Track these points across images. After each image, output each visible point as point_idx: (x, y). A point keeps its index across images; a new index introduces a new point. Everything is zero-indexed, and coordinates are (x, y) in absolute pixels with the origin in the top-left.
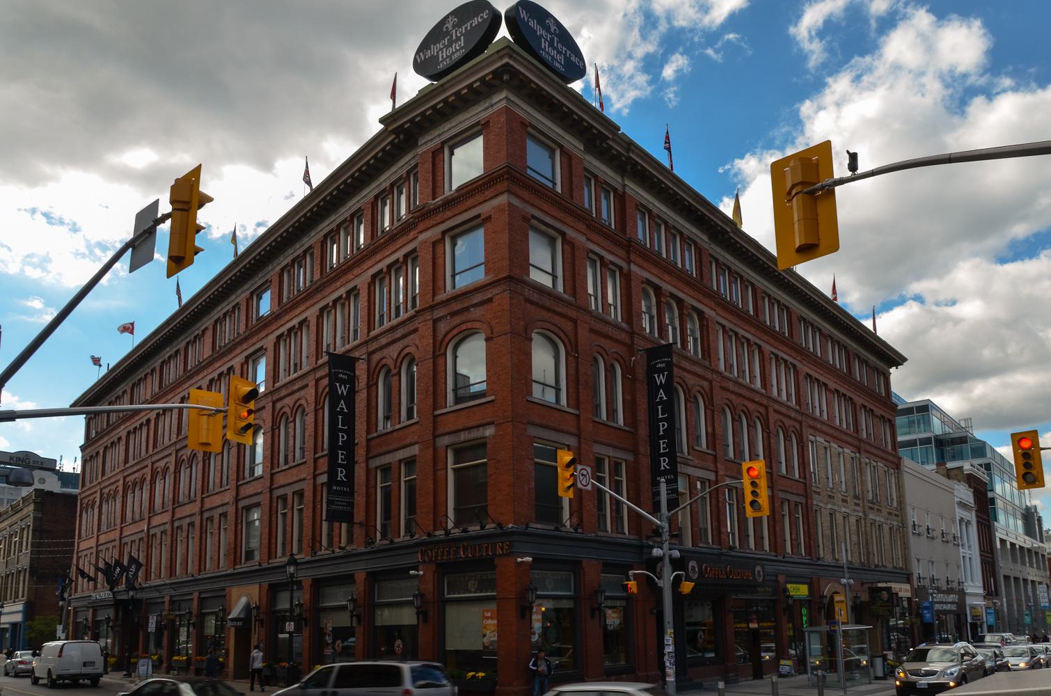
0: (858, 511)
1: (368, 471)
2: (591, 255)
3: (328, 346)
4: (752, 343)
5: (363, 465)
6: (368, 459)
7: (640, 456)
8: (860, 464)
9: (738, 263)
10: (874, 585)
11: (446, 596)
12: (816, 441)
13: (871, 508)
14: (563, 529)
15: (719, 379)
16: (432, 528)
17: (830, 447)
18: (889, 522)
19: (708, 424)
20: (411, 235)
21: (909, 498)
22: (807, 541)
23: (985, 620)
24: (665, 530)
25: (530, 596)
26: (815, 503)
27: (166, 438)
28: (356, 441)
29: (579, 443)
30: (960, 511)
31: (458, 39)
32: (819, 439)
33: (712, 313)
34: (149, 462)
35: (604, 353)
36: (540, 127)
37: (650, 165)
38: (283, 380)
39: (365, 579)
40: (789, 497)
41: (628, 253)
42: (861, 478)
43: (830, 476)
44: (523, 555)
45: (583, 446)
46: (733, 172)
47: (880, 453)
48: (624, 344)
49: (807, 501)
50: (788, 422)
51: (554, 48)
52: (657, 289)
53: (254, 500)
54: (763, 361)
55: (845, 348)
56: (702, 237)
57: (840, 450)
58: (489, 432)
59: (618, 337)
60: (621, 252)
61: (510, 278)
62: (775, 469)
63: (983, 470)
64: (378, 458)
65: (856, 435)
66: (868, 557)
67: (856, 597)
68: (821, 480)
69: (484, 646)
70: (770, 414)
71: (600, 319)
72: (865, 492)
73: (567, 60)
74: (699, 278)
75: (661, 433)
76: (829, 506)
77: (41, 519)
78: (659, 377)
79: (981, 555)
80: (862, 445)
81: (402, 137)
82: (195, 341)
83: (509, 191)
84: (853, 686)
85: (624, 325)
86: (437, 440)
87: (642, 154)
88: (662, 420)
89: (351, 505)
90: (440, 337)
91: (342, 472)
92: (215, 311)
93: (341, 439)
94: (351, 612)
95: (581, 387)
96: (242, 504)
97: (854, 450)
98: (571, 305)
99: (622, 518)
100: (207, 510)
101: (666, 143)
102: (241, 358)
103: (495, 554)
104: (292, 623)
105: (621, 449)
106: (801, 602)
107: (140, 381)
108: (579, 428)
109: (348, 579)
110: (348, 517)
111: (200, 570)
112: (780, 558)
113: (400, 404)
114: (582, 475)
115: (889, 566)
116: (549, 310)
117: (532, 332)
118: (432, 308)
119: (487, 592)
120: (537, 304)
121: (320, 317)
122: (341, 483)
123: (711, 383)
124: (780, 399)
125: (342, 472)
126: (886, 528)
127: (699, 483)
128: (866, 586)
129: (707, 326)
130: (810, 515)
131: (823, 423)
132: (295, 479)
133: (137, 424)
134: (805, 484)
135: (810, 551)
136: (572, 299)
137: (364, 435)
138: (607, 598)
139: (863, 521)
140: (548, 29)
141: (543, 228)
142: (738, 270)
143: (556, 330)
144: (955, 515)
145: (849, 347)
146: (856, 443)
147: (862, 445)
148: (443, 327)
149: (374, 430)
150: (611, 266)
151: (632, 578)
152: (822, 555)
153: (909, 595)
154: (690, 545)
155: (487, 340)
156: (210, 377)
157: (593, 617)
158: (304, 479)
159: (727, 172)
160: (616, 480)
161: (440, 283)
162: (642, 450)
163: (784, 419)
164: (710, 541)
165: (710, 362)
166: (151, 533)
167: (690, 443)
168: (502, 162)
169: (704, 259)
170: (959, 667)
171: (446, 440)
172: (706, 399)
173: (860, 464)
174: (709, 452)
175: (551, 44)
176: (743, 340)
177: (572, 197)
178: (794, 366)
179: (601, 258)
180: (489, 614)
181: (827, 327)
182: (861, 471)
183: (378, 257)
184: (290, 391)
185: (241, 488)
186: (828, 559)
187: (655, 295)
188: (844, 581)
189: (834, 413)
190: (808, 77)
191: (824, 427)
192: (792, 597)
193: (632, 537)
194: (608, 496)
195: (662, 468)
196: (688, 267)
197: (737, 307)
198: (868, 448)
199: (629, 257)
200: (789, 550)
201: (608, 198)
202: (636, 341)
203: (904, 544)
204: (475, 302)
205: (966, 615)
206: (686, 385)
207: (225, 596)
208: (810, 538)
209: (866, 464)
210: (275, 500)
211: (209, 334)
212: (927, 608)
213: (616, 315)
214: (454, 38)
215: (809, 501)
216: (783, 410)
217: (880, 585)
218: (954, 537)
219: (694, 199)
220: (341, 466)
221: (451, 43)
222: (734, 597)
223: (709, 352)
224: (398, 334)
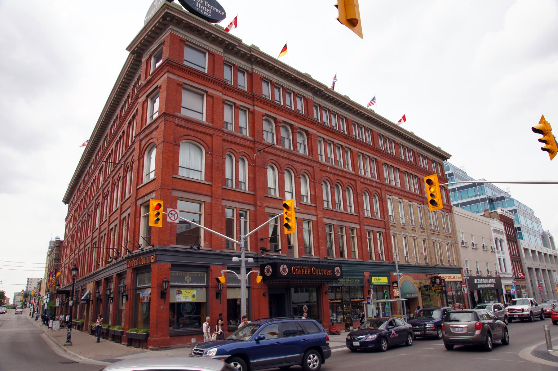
0: (424, 236)
7: (258, 207)
8: (424, 210)
11: (138, 286)
12: (393, 199)
18: (445, 241)
21: (458, 228)
29: (212, 200)
30: (496, 234)
33: (315, 132)
37: (265, 58)
40: (372, 228)
41: (253, 101)
42: (425, 218)
48: (249, 148)
49: (386, 231)
51: (204, 6)
57: (410, 203)
59: (245, 144)
60: (250, 101)
61: (164, 114)
62: (361, 214)
66: (431, 260)
83: (168, 71)
87: (259, 53)
95: (213, 170)
97: (420, 203)
103: (150, 262)
108: (212, 192)
114: (172, 214)
116: (193, 130)
117: (267, 165)
120: (184, 127)
129: (311, 138)
141: (194, 90)
142: (392, 138)
143: (199, 140)
145: (414, 150)
150: (337, 145)
154: (298, 257)
165: (313, 157)
174: (356, 214)
179: (333, 142)
181: (398, 140)
182: (425, 214)
203: (457, 252)
213: (246, 133)
215: (387, 231)
223: (312, 152)
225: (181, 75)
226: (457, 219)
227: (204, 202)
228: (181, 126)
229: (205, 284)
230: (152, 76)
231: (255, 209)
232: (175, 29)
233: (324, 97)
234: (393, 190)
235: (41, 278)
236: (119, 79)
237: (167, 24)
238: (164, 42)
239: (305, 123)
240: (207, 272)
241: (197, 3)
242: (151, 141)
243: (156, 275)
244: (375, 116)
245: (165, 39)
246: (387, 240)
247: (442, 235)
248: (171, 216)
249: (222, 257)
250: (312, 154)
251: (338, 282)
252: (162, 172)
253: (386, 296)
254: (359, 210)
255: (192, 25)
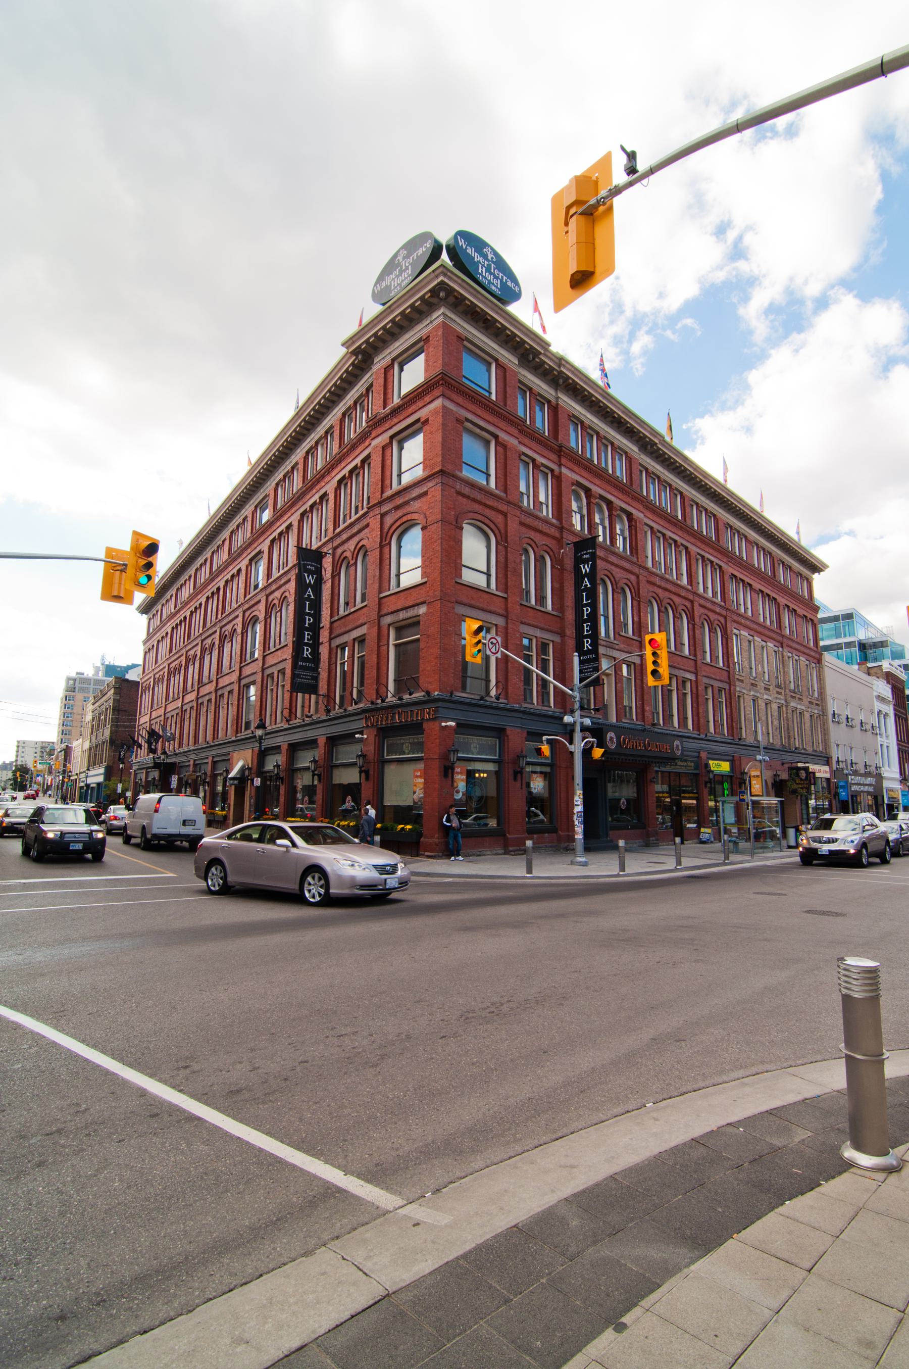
0: (780, 699)
1: (330, 649)
2: (523, 457)
3: (307, 545)
4: (679, 544)
5: (327, 644)
6: (331, 639)
7: (566, 638)
8: (783, 657)
9: (666, 473)
10: (794, 765)
11: (386, 757)
12: (740, 635)
13: (793, 697)
14: (487, 698)
15: (646, 574)
16: (374, 697)
17: (754, 640)
18: (810, 710)
19: (635, 613)
20: (367, 443)
21: (829, 690)
22: (729, 722)
23: (901, 802)
24: (577, 699)
25: (453, 758)
26: (738, 689)
27: (197, 631)
28: (321, 625)
29: (507, 623)
30: (879, 704)
31: (407, 268)
32: (743, 632)
33: (641, 516)
34: (184, 651)
35: (534, 545)
36: (476, 341)
38: (275, 575)
39: (325, 744)
40: (712, 682)
41: (560, 457)
42: (784, 669)
43: (753, 667)
44: (447, 720)
45: (510, 626)
46: (694, 429)
47: (802, 649)
48: (554, 538)
50: (713, 616)
51: (491, 273)
52: (588, 492)
53: (251, 679)
54: (690, 561)
55: (770, 554)
56: (632, 448)
57: (764, 644)
58: (422, 610)
59: (548, 531)
60: (554, 457)
61: (442, 472)
62: (699, 657)
63: (902, 670)
64: (338, 638)
65: (779, 631)
66: (789, 740)
67: (775, 775)
68: (744, 669)
69: (414, 802)
70: (695, 608)
71: (530, 514)
72: (787, 682)
73: (504, 285)
74: (628, 484)
75: (585, 617)
76: (752, 693)
77: (119, 701)
78: (584, 567)
79: (898, 745)
80: (785, 640)
81: (360, 357)
82: (218, 550)
83: (443, 395)
84: (763, 853)
85: (554, 521)
86: (382, 619)
87: (573, 369)
88: (586, 605)
89: (316, 679)
90: (386, 528)
91: (307, 650)
92: (231, 524)
93: (307, 622)
94: (313, 771)
95: (509, 573)
96: (243, 682)
97: (777, 644)
98: (502, 499)
99: (548, 693)
100: (220, 689)
101: (601, 365)
102: (246, 561)
103: (423, 719)
104: (259, 779)
105: (547, 630)
106: (721, 778)
107: (182, 585)
108: (506, 609)
109: (311, 743)
110: (312, 689)
111: (214, 739)
112: (702, 736)
113: (355, 590)
114: (492, 643)
115: (810, 750)
118: (380, 503)
119: (418, 753)
120: (468, 497)
121: (301, 521)
122: (307, 660)
123: (638, 577)
124: (705, 595)
125: (307, 650)
126: (807, 715)
127: (624, 667)
128: (786, 766)
130: (733, 702)
131: (747, 618)
132: (280, 659)
133: (178, 621)
134: (729, 672)
135: (733, 732)
136: (503, 495)
137: (328, 619)
138: (528, 764)
139: (784, 709)
140: (485, 257)
141: (478, 431)
142: (743, 532)
143: (480, 518)
144: (873, 705)
145: (773, 554)
146: (780, 638)
147: (785, 640)
148: (389, 520)
149: (336, 614)
150: (542, 468)
151: (545, 743)
152: (744, 736)
153: (828, 776)
154: (614, 720)
155: (423, 529)
156: (225, 579)
157: (515, 779)
158: (286, 660)
159: (689, 429)
160: (542, 659)
161: (388, 482)
162: (568, 632)
163: (709, 614)
164: (634, 718)
165: (638, 558)
166: (184, 709)
167: (616, 629)
168: (438, 369)
169: (634, 467)
170: (860, 835)
171: (388, 620)
172: (633, 591)
173: (783, 657)
175: (488, 269)
176: (671, 541)
177: (506, 405)
178: (720, 567)
179: (534, 460)
180: (418, 774)
181: (753, 535)
183: (343, 464)
184: (278, 585)
185: (243, 669)
186: (750, 740)
187: (586, 497)
188: (759, 757)
189: (758, 610)
190: (755, 348)
191: (748, 623)
192: (712, 772)
193: (557, 710)
194: (534, 675)
195: (586, 649)
196: (618, 474)
197: (666, 512)
198: (791, 643)
199: (560, 461)
200: (712, 730)
201: (542, 410)
202: (565, 535)
203: (824, 730)
204: (414, 495)
205: (883, 797)
206: (614, 578)
207: (229, 759)
208: (732, 721)
209: (789, 658)
210: (265, 679)
211: (227, 543)
212: (842, 787)
213: (547, 512)
214: (404, 268)
216: (709, 605)
217: (800, 765)
218: (873, 727)
219: (623, 412)
220: (307, 644)
221: (401, 272)
222: (656, 769)
223: (637, 550)
224: (355, 529)
225: (461, 404)
226: (828, 674)
227: (496, 625)
228: (464, 496)
229: (497, 757)
230: (405, 400)
231: (562, 640)
232: (449, 315)
233: (654, 455)
234: (743, 621)
235: (53, 743)
236: (312, 399)
237: (434, 304)
238: (429, 336)
239: (629, 500)
240: (499, 738)
241: (480, 266)
242: (409, 517)
243: (437, 741)
244: (726, 493)
245: (430, 332)
246: (731, 703)
247: (806, 701)
248: (491, 646)
249: (521, 715)
250: (637, 553)
251: (676, 765)
252: (441, 573)
253: (726, 792)
254: (695, 650)
255: (479, 310)
